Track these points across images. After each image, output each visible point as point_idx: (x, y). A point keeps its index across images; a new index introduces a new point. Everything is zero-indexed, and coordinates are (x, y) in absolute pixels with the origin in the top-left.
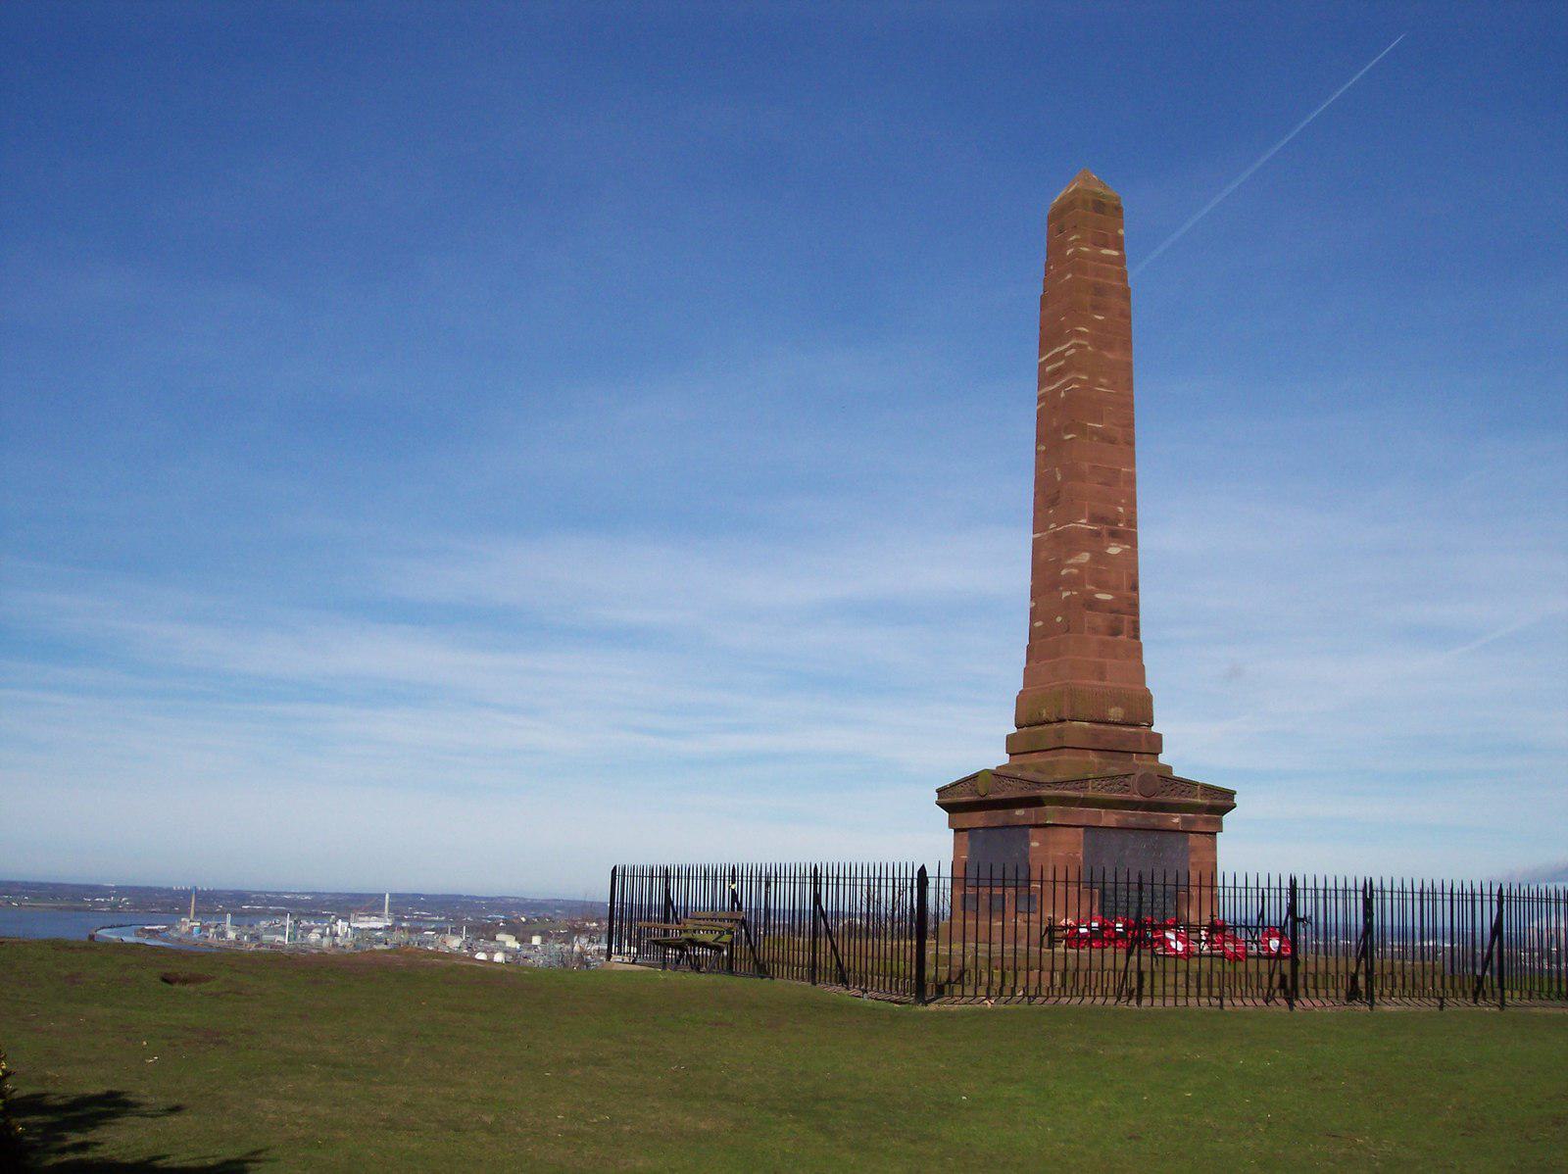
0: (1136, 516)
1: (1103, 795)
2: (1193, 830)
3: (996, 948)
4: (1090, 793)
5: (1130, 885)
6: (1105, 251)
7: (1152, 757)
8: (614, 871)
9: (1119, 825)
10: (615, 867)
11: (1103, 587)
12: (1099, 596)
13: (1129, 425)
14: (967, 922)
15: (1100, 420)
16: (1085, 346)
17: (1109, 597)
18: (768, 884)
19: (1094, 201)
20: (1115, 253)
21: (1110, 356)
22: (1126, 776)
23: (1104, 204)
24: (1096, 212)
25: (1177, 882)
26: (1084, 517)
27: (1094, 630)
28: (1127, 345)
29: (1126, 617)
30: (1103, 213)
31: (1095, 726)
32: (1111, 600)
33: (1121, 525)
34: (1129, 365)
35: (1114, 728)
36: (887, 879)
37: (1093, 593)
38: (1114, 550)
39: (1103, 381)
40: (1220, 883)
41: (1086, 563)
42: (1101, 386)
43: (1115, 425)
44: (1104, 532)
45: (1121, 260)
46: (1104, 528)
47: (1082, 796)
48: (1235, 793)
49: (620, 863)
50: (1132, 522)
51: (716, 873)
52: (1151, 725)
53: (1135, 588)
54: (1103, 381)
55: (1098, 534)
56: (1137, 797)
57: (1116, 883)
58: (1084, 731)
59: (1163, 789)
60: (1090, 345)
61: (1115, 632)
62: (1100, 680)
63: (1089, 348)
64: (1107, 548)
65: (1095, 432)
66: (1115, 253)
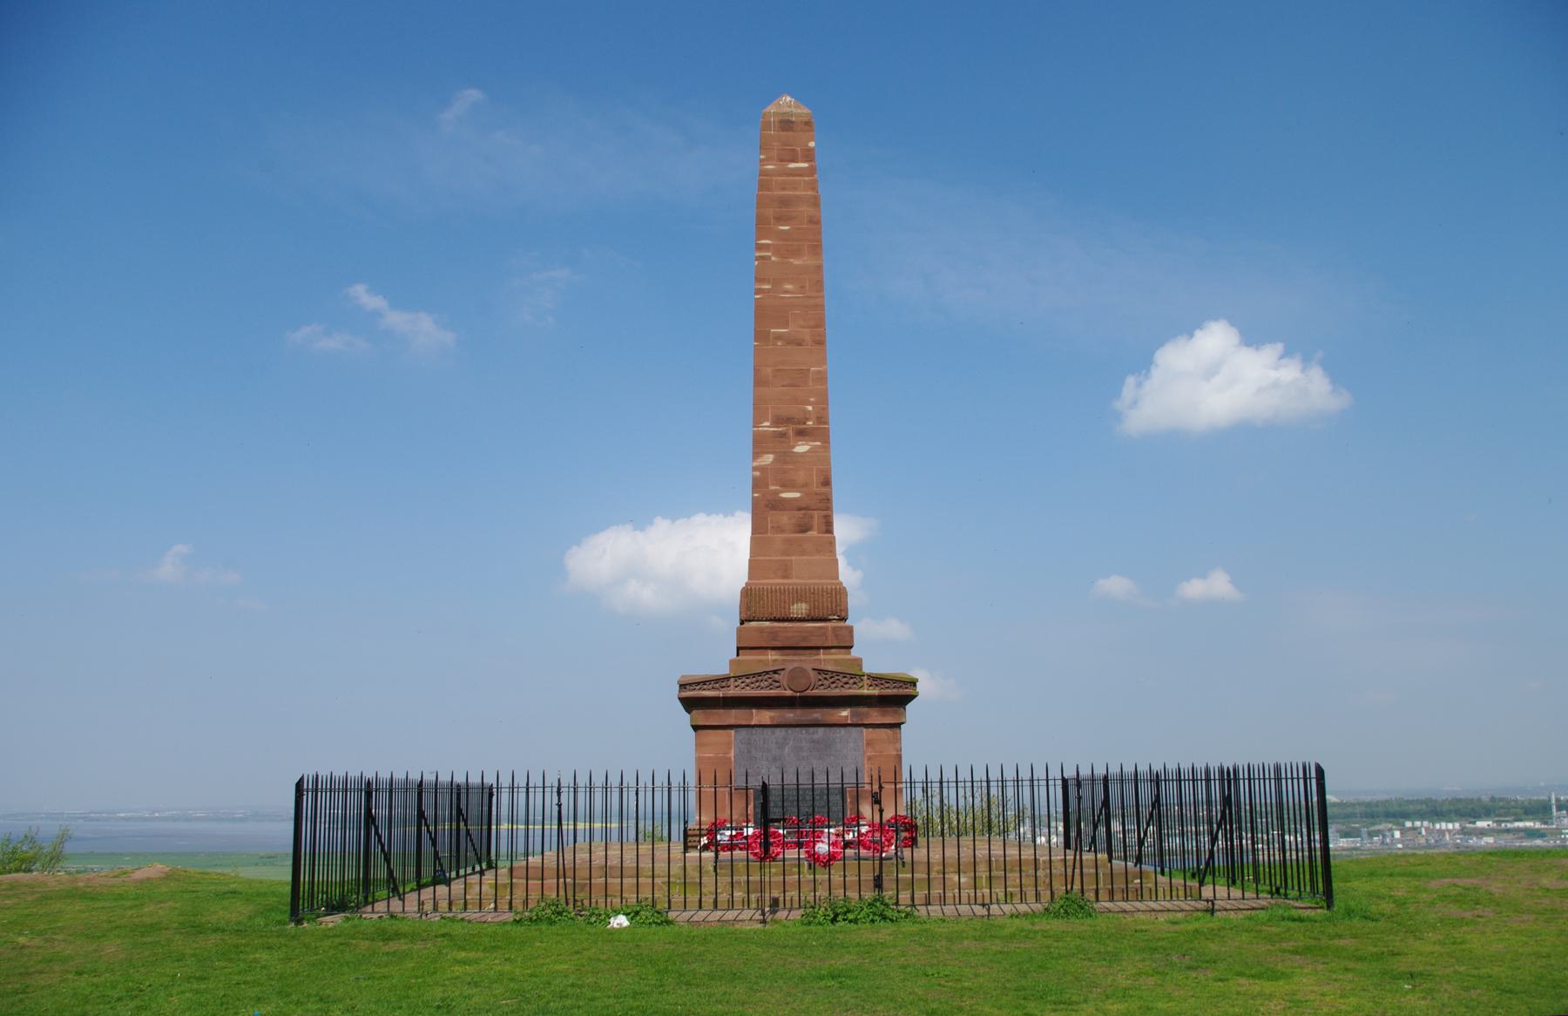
0: (828, 414)
1: (749, 692)
2: (866, 722)
3: (614, 852)
4: (732, 692)
5: (959, 784)
6: (792, 165)
7: (846, 650)
8: (299, 786)
9: (775, 723)
10: (301, 780)
11: (788, 485)
12: (784, 495)
13: (819, 323)
14: (545, 827)
15: (786, 325)
16: (770, 257)
17: (797, 495)
18: (491, 795)
19: (781, 122)
20: (805, 165)
21: (796, 262)
22: (775, 672)
23: (792, 122)
24: (783, 130)
25: (544, 784)
26: (768, 421)
27: (779, 529)
28: (816, 249)
29: (816, 512)
30: (793, 131)
31: (776, 624)
32: (800, 497)
33: (810, 423)
34: (819, 268)
35: (798, 624)
36: (1286, 779)
37: (776, 493)
38: (801, 448)
39: (789, 287)
40: (905, 776)
41: (769, 465)
42: (787, 292)
43: (803, 327)
44: (791, 433)
45: (812, 171)
46: (790, 430)
47: (721, 695)
48: (917, 680)
49: (309, 772)
50: (822, 419)
51: (317, 786)
52: (844, 619)
53: (827, 483)
54: (789, 287)
55: (783, 435)
56: (789, 693)
57: (828, 784)
58: (761, 630)
59: (820, 683)
60: (773, 254)
61: (804, 528)
62: (784, 577)
63: (773, 258)
64: (794, 447)
65: (779, 337)
66: (805, 165)
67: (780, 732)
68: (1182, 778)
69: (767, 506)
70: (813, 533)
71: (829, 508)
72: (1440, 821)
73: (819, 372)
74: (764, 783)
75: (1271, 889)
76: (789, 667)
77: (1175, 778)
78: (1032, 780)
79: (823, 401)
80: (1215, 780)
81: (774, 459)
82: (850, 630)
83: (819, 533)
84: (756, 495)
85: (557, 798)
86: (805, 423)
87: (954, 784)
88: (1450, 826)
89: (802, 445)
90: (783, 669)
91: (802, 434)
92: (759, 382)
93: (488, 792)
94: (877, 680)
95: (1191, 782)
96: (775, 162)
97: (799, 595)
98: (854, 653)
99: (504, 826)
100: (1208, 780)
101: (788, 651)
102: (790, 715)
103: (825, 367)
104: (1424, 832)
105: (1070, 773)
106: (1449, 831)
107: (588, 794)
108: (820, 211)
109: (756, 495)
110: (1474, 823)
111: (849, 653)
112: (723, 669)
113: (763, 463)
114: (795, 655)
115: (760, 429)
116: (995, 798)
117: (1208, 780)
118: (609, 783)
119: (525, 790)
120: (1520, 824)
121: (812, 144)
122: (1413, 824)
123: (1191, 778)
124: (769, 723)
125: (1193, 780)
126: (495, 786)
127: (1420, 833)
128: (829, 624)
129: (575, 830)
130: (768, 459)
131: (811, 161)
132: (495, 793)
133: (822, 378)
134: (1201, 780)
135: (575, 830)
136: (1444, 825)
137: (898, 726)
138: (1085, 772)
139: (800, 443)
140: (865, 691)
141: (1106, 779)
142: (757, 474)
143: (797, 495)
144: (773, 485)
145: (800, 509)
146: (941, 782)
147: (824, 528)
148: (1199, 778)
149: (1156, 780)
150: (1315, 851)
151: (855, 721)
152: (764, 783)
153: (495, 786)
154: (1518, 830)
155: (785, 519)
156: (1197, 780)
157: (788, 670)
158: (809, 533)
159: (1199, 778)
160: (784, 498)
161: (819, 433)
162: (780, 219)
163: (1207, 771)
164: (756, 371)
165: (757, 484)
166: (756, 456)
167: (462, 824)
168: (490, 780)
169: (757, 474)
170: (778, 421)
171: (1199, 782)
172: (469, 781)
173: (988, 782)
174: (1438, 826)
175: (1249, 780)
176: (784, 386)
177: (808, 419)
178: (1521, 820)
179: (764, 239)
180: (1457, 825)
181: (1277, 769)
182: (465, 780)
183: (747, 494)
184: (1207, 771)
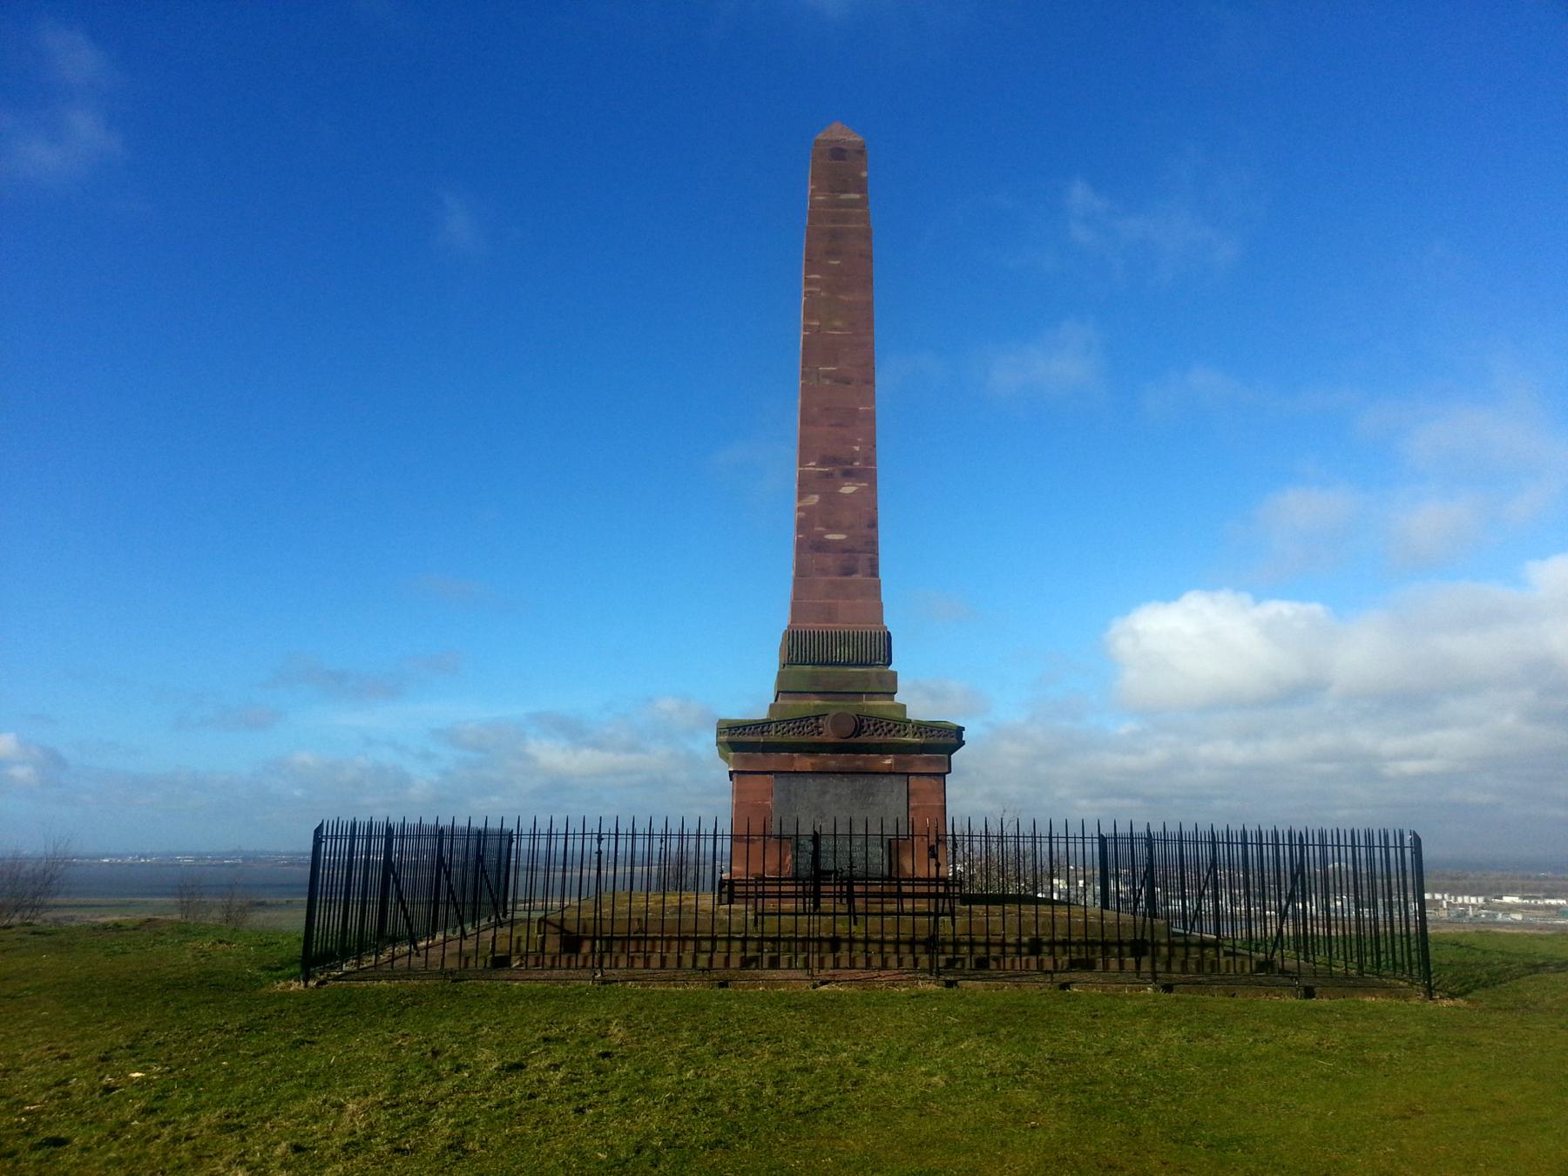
4: (773, 737)
6: (844, 196)
11: (832, 528)
12: (829, 537)
17: (842, 537)
18: (511, 841)
32: (847, 538)
33: (857, 464)
37: (822, 534)
38: (848, 489)
39: (838, 323)
45: (863, 203)
50: (870, 460)
53: (873, 525)
54: (838, 323)
55: (828, 475)
61: (848, 571)
67: (821, 781)
68: (1264, 841)
69: (811, 547)
70: (857, 577)
71: (875, 552)
72: (1463, 894)
73: (867, 412)
74: (815, 832)
75: (1152, 921)
76: (833, 713)
77: (1254, 841)
78: (1051, 837)
79: (872, 444)
80: (1284, 845)
81: (820, 500)
82: (894, 675)
83: (863, 576)
84: (800, 536)
85: (597, 845)
86: (852, 464)
87: (1064, 840)
88: (1473, 900)
89: (848, 486)
90: (826, 715)
91: (849, 474)
92: (806, 420)
93: (507, 837)
94: (922, 727)
95: (1225, 845)
96: (827, 193)
97: (844, 639)
98: (898, 699)
99: (522, 876)
100: (1245, 844)
101: (830, 696)
102: (833, 762)
103: (873, 407)
104: (1445, 905)
105: (1107, 831)
106: (1473, 905)
107: (532, 840)
108: (871, 245)
109: (800, 536)
110: (1501, 898)
111: (893, 700)
112: (762, 714)
113: (808, 504)
114: (836, 700)
115: (807, 469)
116: (995, 855)
117: (1245, 844)
118: (669, 830)
119: (564, 836)
120: (1553, 902)
121: (864, 174)
122: (1434, 897)
123: (1225, 841)
124: (810, 770)
125: (1228, 843)
126: (515, 832)
127: (1442, 906)
128: (874, 669)
129: (632, 873)
130: (814, 499)
131: (863, 192)
132: (515, 840)
133: (871, 418)
134: (1284, 845)
135: (632, 873)
136: (1466, 899)
137: (943, 775)
138: (1156, 829)
139: (846, 484)
140: (909, 739)
141: (816, 838)
142: (803, 514)
143: (842, 537)
144: (820, 526)
145: (845, 551)
146: (1051, 837)
147: (869, 571)
148: (1220, 840)
149: (1149, 840)
150: (1323, 925)
151: (899, 769)
152: (815, 832)
153: (515, 832)
154: (1549, 907)
155: (830, 561)
156: (1218, 843)
157: (832, 715)
158: (853, 576)
159: (1220, 840)
160: (829, 540)
161: (867, 474)
162: (831, 253)
163: (1244, 833)
164: (804, 410)
165: (802, 526)
166: (801, 496)
167: (443, 876)
168: (510, 825)
169: (803, 514)
170: (823, 462)
171: (1221, 845)
172: (504, 827)
173: (617, 835)
174: (1460, 900)
175: (1353, 846)
176: (832, 426)
177: (855, 460)
178: (1553, 898)
179: (814, 274)
180: (1481, 900)
181: (1322, 835)
182: (484, 826)
183: (790, 536)
184: (1244, 833)
